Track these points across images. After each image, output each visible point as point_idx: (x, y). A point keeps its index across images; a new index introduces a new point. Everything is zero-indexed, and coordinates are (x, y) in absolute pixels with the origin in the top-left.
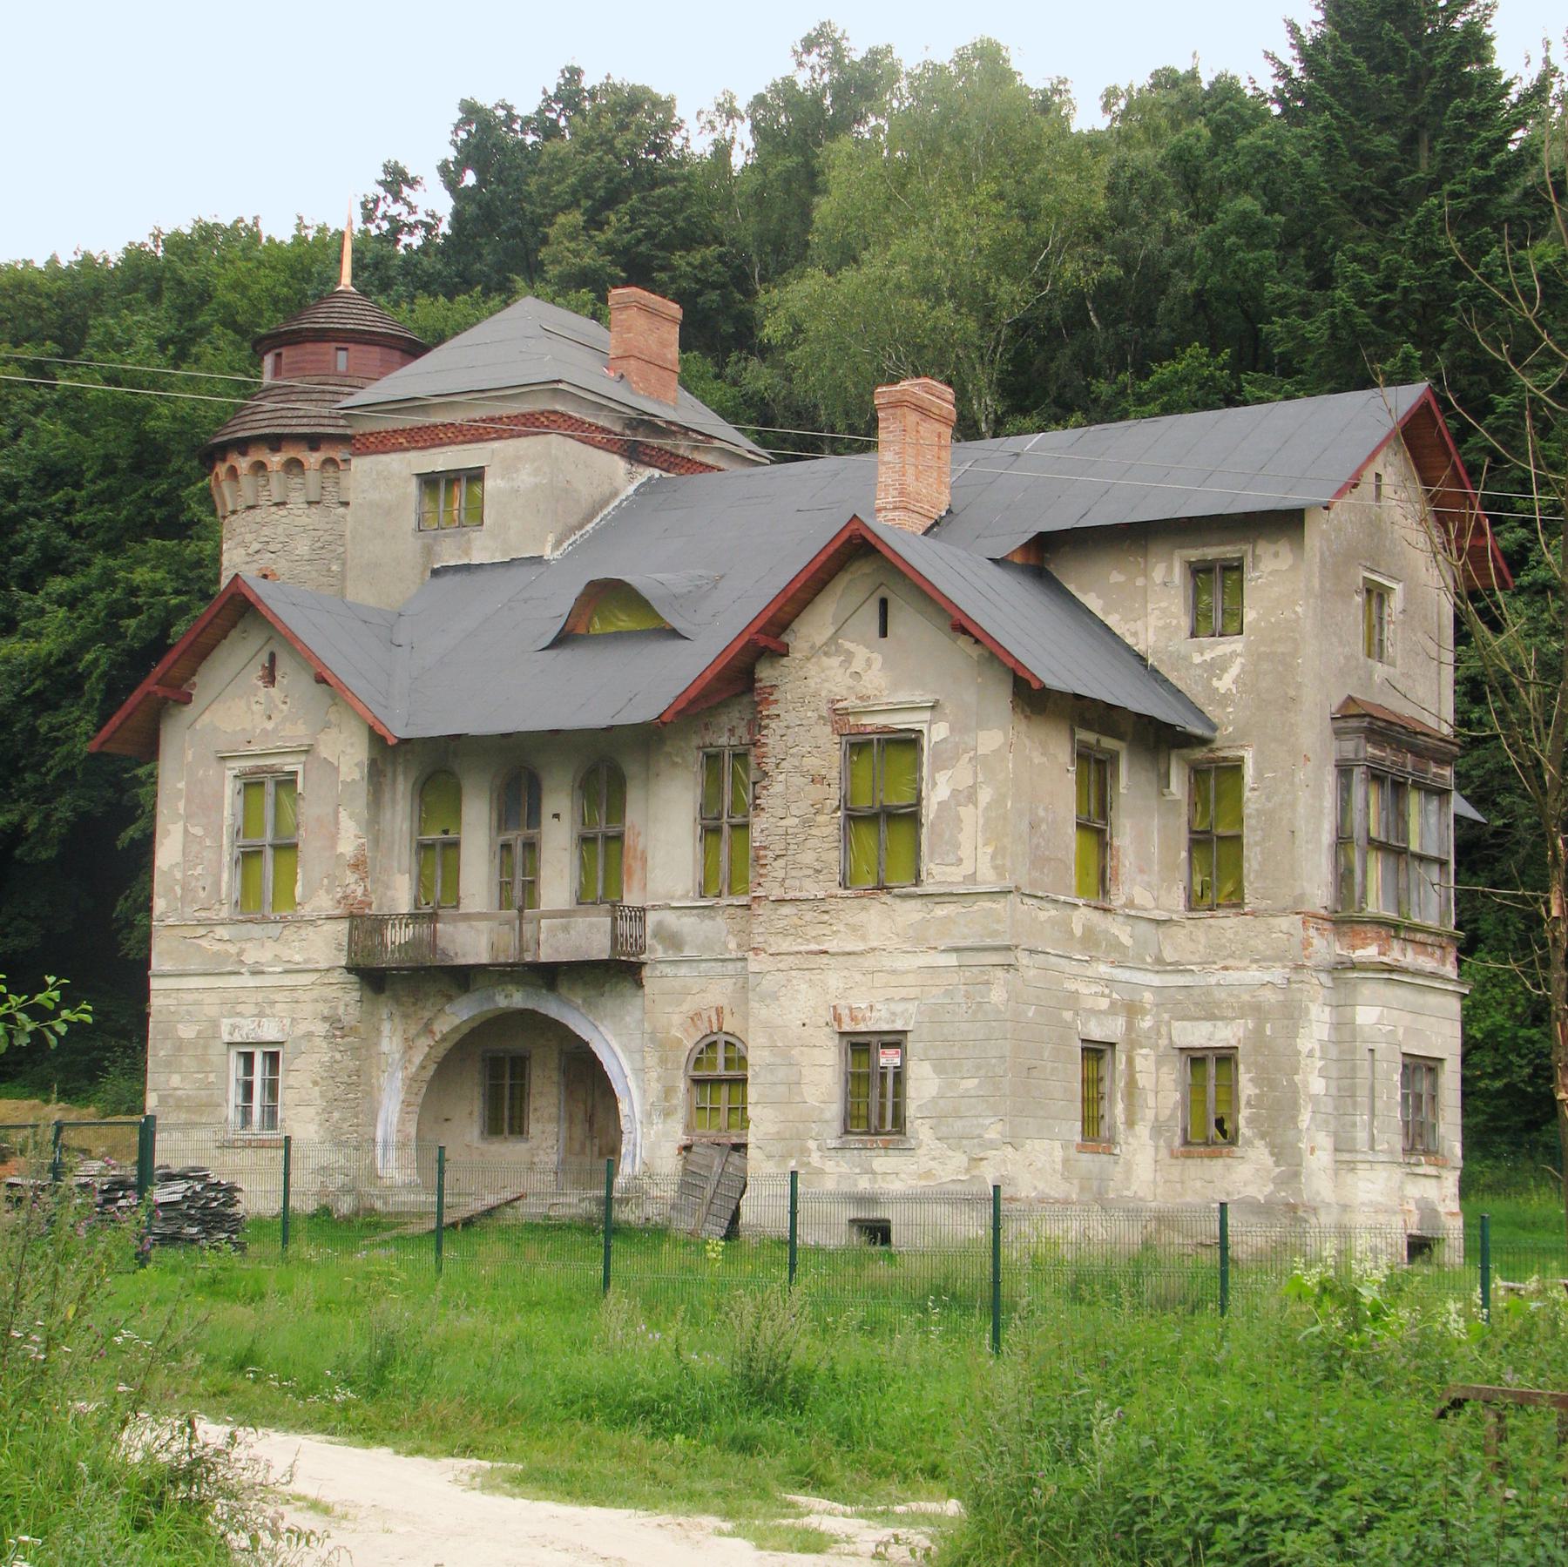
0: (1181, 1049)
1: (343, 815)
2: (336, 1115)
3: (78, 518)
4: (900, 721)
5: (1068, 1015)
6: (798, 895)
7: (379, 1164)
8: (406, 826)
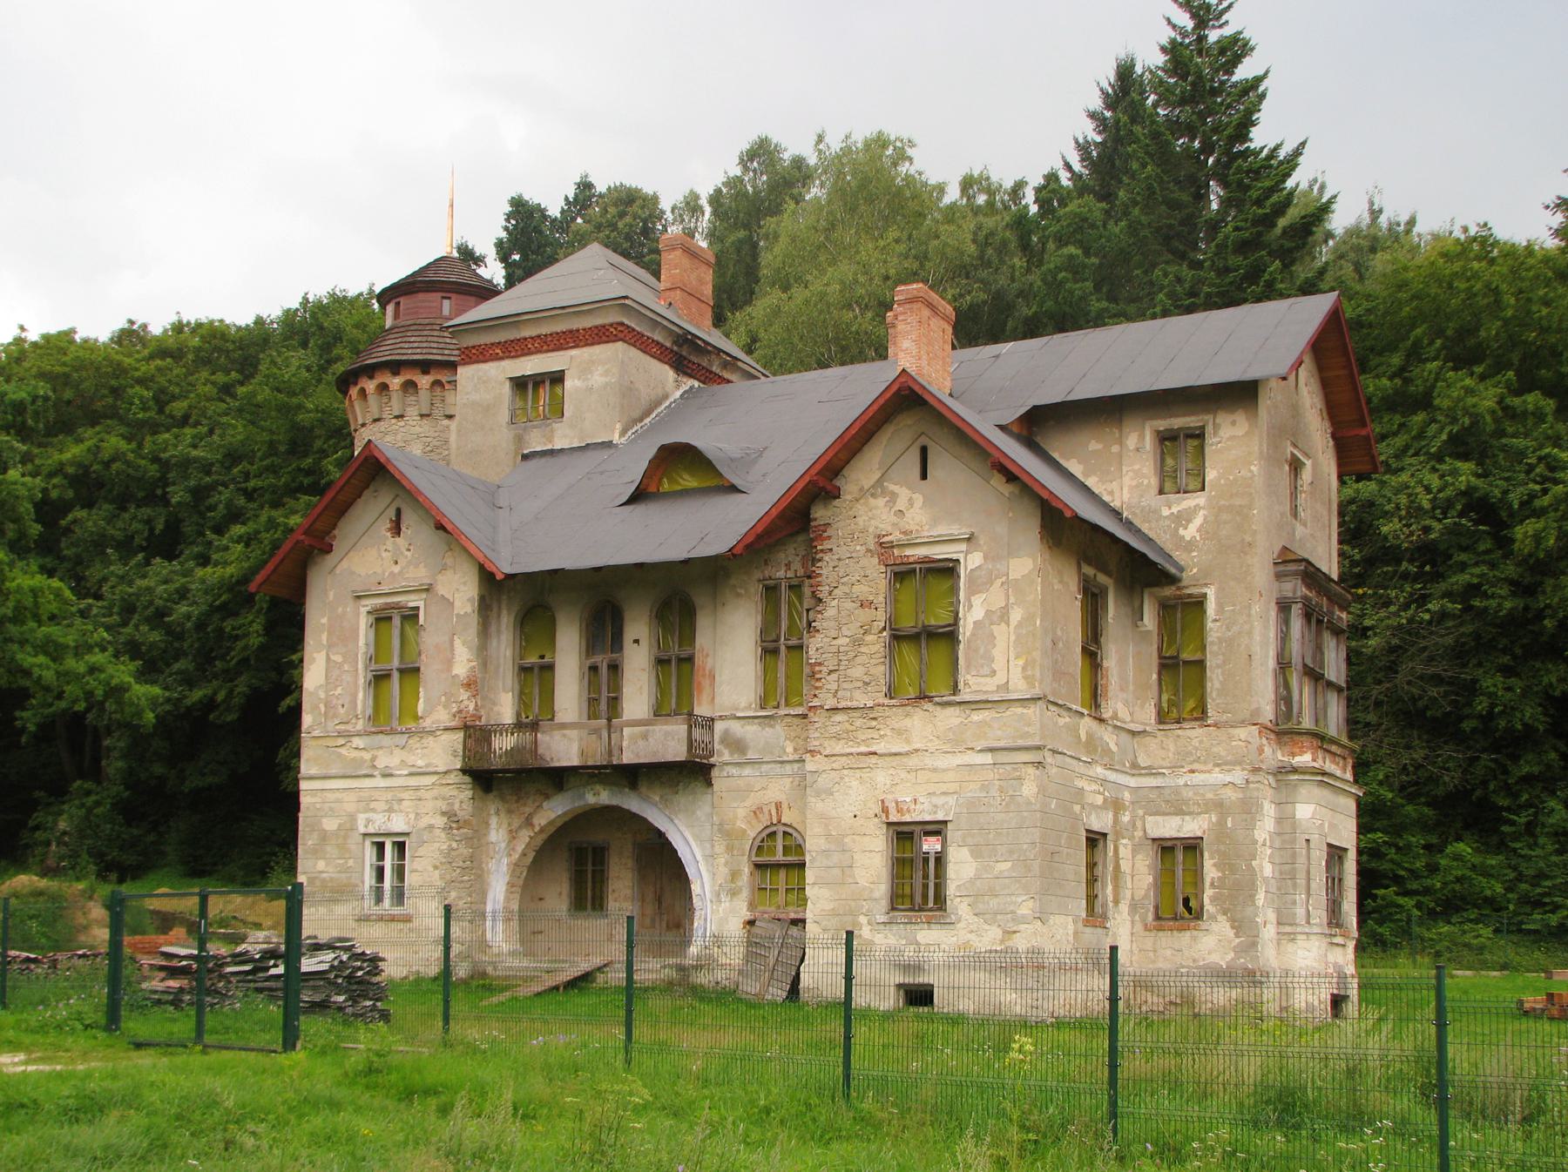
0: (1154, 840)
1: (458, 642)
3: (252, 484)
4: (939, 552)
5: (1077, 808)
6: (849, 704)
7: (489, 936)
8: (509, 653)
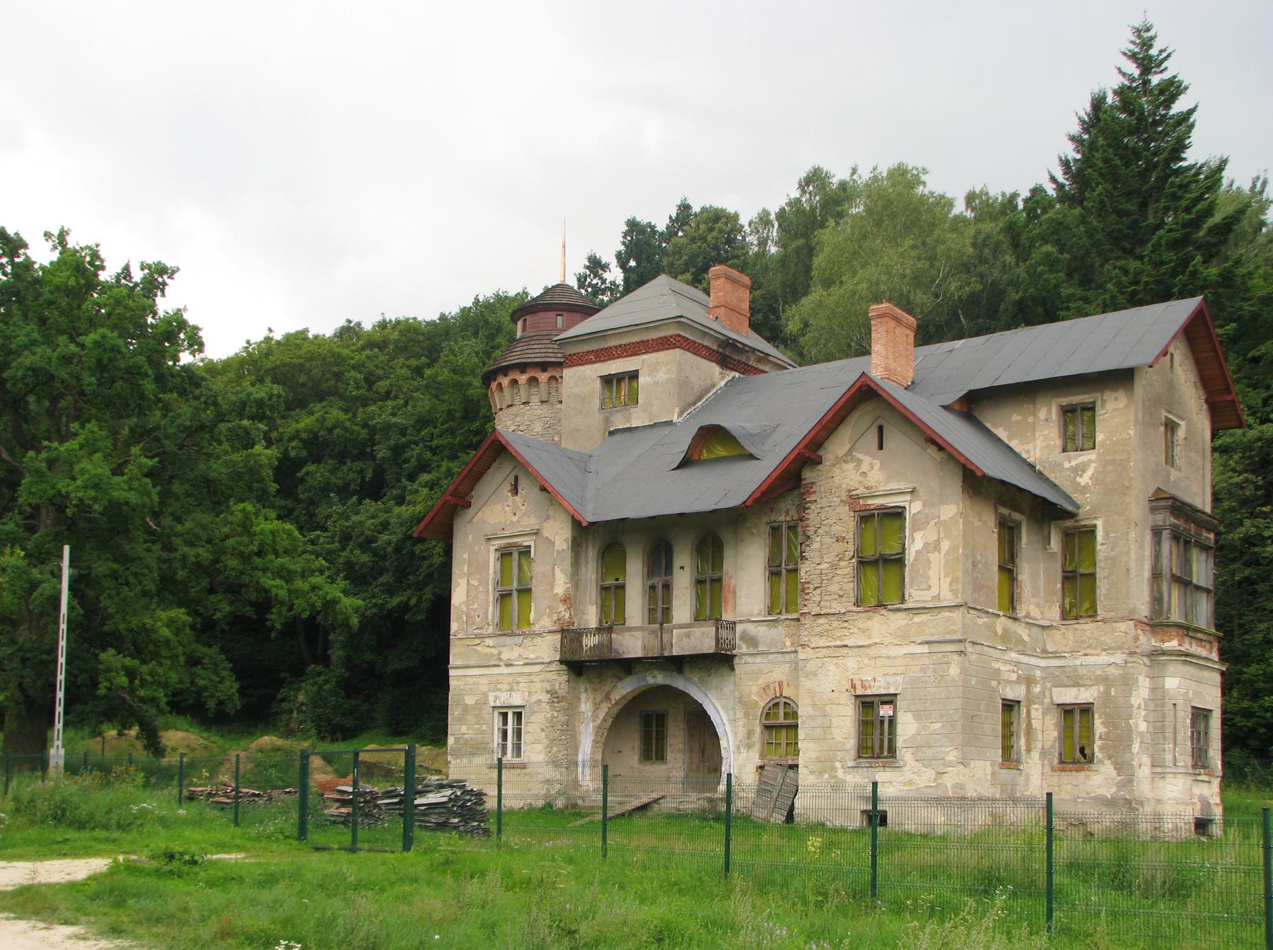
1: (557, 570)
2: (555, 749)
3: (435, 443)
4: (891, 502)
5: (994, 683)
6: (829, 611)
8: (594, 577)
